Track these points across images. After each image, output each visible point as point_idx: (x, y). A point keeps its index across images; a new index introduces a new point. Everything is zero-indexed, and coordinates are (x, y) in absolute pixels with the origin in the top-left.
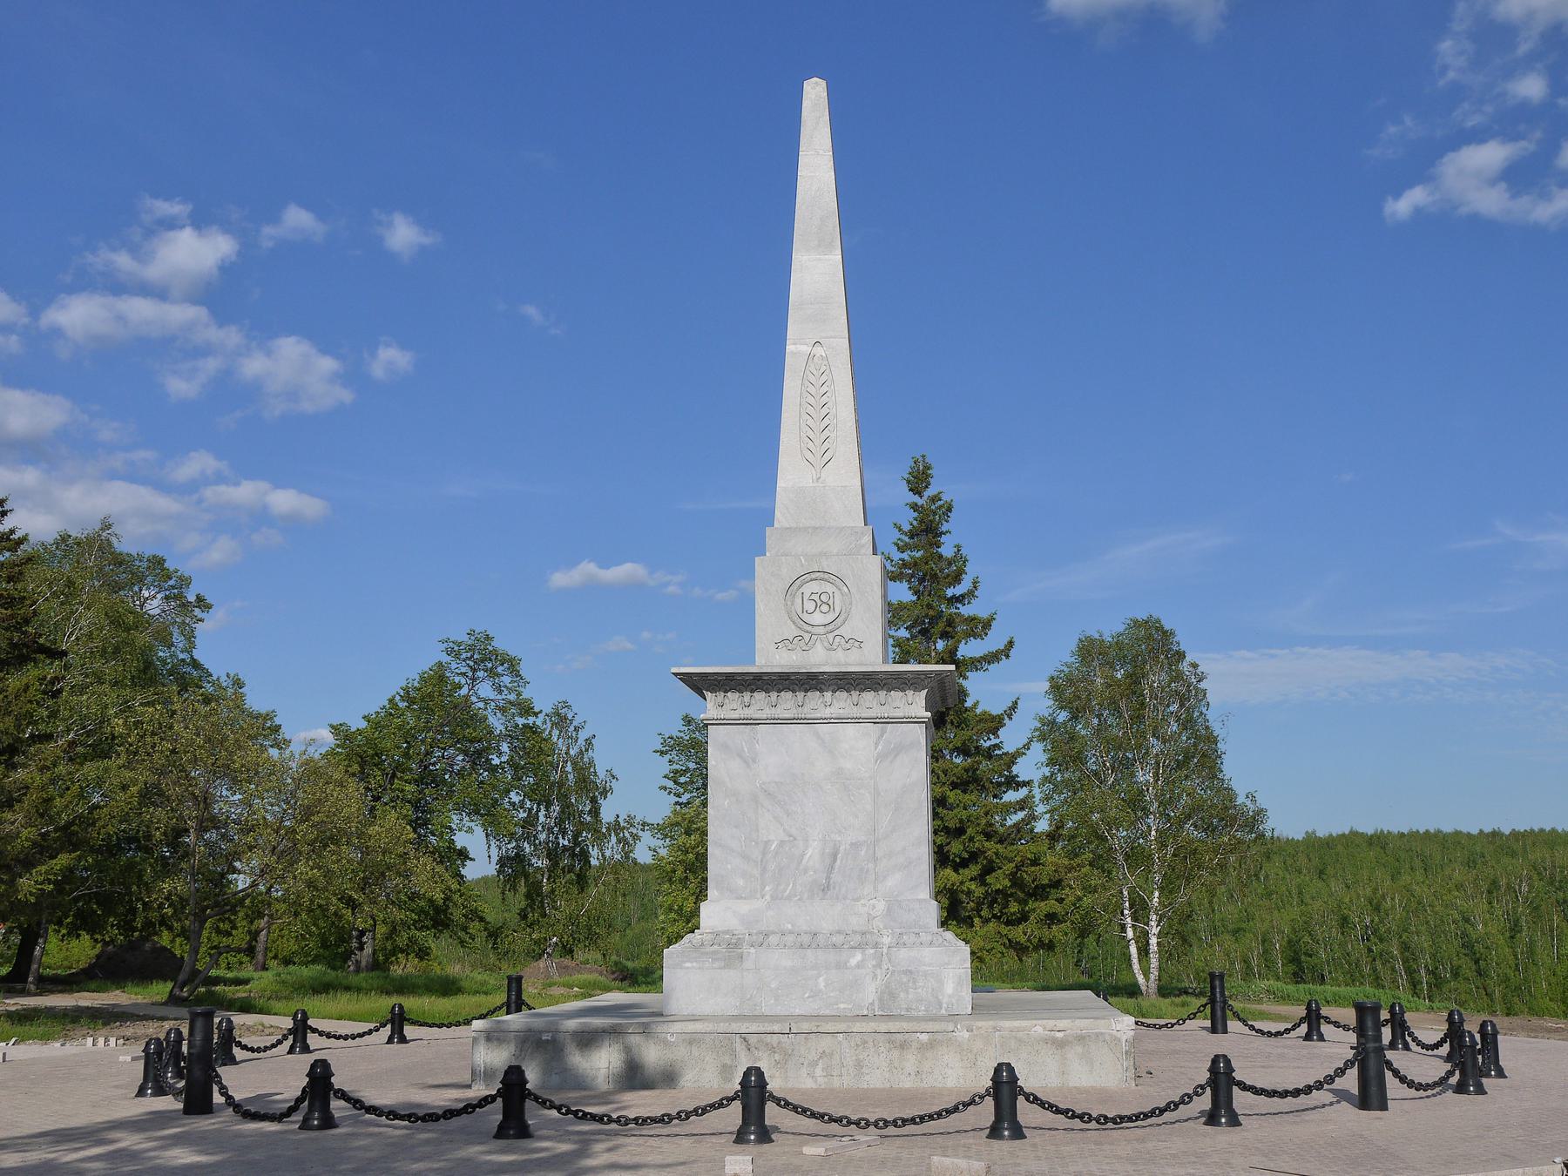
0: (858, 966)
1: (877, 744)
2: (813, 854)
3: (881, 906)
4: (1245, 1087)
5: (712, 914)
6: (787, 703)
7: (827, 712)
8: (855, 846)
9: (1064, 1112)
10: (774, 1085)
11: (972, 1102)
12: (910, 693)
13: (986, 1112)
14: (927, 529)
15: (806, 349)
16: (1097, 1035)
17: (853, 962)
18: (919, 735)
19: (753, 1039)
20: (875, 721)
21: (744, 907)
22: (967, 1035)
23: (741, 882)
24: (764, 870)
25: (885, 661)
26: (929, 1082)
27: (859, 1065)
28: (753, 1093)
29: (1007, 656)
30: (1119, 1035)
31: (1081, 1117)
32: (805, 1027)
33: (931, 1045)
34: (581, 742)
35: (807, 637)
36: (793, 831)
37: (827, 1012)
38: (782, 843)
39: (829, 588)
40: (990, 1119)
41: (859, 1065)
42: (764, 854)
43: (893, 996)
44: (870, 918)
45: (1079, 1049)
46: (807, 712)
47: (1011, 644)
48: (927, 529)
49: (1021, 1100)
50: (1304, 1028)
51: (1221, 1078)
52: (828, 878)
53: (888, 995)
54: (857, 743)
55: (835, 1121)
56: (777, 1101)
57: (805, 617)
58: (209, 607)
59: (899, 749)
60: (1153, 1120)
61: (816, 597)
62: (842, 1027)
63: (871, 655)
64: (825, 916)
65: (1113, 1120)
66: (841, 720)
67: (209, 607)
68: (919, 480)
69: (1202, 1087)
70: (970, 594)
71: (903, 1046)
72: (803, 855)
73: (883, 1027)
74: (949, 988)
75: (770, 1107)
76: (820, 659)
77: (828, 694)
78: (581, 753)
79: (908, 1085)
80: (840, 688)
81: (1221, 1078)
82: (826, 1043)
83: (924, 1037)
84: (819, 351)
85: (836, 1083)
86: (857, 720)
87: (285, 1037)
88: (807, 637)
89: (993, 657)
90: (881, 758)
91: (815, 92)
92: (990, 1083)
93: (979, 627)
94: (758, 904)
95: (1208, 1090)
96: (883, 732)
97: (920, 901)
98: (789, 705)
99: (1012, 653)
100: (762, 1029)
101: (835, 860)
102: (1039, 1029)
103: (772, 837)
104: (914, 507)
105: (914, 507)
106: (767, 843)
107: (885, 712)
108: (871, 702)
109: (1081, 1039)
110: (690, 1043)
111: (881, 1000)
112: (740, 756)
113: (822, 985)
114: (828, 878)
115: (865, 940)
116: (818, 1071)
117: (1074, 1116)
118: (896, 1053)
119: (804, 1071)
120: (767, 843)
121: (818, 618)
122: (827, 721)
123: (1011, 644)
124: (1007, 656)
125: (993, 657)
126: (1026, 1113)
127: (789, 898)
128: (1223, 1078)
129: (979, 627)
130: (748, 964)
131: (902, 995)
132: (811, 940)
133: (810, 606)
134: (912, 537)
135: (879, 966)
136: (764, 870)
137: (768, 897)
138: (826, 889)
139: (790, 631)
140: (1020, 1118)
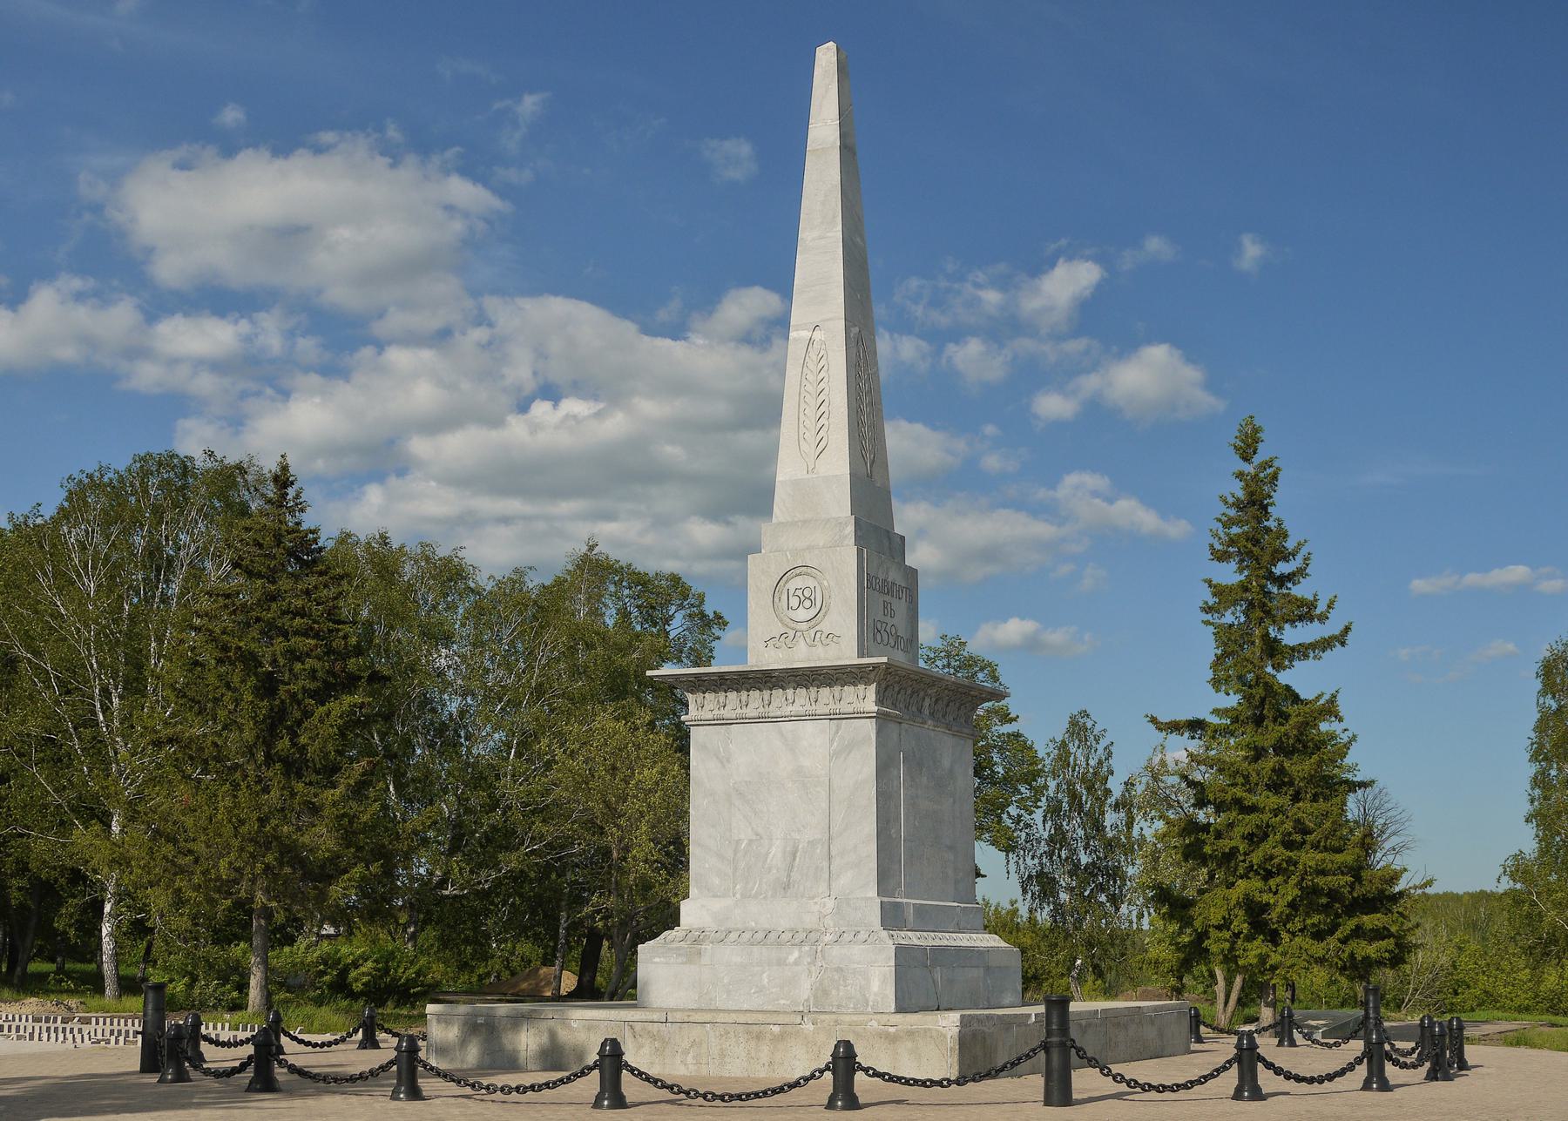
0: (796, 963)
1: (832, 741)
2: (776, 852)
3: (830, 903)
5: (691, 912)
6: (755, 701)
7: (788, 710)
14: (1255, 502)
15: (806, 334)
16: (926, 1030)
17: (792, 959)
18: (870, 727)
19: (638, 1027)
20: (833, 717)
21: (717, 905)
22: (812, 1027)
23: (717, 881)
24: (735, 869)
25: (861, 655)
27: (722, 1055)
29: (1343, 644)
30: (944, 1031)
31: (671, 1088)
32: (679, 1017)
33: (782, 1037)
34: (1101, 748)
38: (751, 841)
39: (811, 583)
41: (722, 1055)
42: (736, 852)
43: (826, 993)
44: (821, 917)
45: (909, 1044)
46: (773, 711)
47: (1347, 629)
48: (1255, 502)
52: (789, 876)
53: (822, 992)
58: (726, 624)
60: (756, 1102)
61: (799, 593)
62: (707, 1017)
63: (845, 652)
64: (783, 914)
65: (722, 1098)
66: (800, 718)
67: (726, 624)
68: (1247, 446)
70: (1301, 572)
71: (759, 1037)
72: (768, 853)
74: (875, 986)
75: (859, 1077)
76: (801, 656)
77: (790, 692)
78: (1100, 762)
79: (762, 1075)
80: (799, 685)
82: (696, 1031)
83: (776, 1029)
84: (818, 335)
85: (704, 1072)
86: (814, 717)
89: (1326, 644)
90: (834, 755)
91: (826, 57)
93: (1305, 612)
94: (729, 902)
96: (838, 728)
98: (853, 698)
99: (1350, 638)
100: (644, 1018)
102: (874, 1023)
104: (1240, 475)
105: (1240, 475)
106: (738, 842)
107: (845, 708)
108: (826, 698)
109: (911, 1034)
111: (815, 997)
114: (789, 876)
115: (806, 938)
116: (690, 1059)
117: (663, 1086)
118: (753, 1043)
119: (678, 1059)
121: (802, 614)
123: (1347, 629)
124: (1343, 644)
125: (1326, 644)
126: (630, 1087)
129: (1305, 612)
130: (705, 960)
131: (834, 992)
132: (766, 937)
133: (794, 602)
134: (1240, 509)
135: (813, 963)
136: (735, 869)
138: (786, 887)
139: (778, 629)
140: (857, 1090)
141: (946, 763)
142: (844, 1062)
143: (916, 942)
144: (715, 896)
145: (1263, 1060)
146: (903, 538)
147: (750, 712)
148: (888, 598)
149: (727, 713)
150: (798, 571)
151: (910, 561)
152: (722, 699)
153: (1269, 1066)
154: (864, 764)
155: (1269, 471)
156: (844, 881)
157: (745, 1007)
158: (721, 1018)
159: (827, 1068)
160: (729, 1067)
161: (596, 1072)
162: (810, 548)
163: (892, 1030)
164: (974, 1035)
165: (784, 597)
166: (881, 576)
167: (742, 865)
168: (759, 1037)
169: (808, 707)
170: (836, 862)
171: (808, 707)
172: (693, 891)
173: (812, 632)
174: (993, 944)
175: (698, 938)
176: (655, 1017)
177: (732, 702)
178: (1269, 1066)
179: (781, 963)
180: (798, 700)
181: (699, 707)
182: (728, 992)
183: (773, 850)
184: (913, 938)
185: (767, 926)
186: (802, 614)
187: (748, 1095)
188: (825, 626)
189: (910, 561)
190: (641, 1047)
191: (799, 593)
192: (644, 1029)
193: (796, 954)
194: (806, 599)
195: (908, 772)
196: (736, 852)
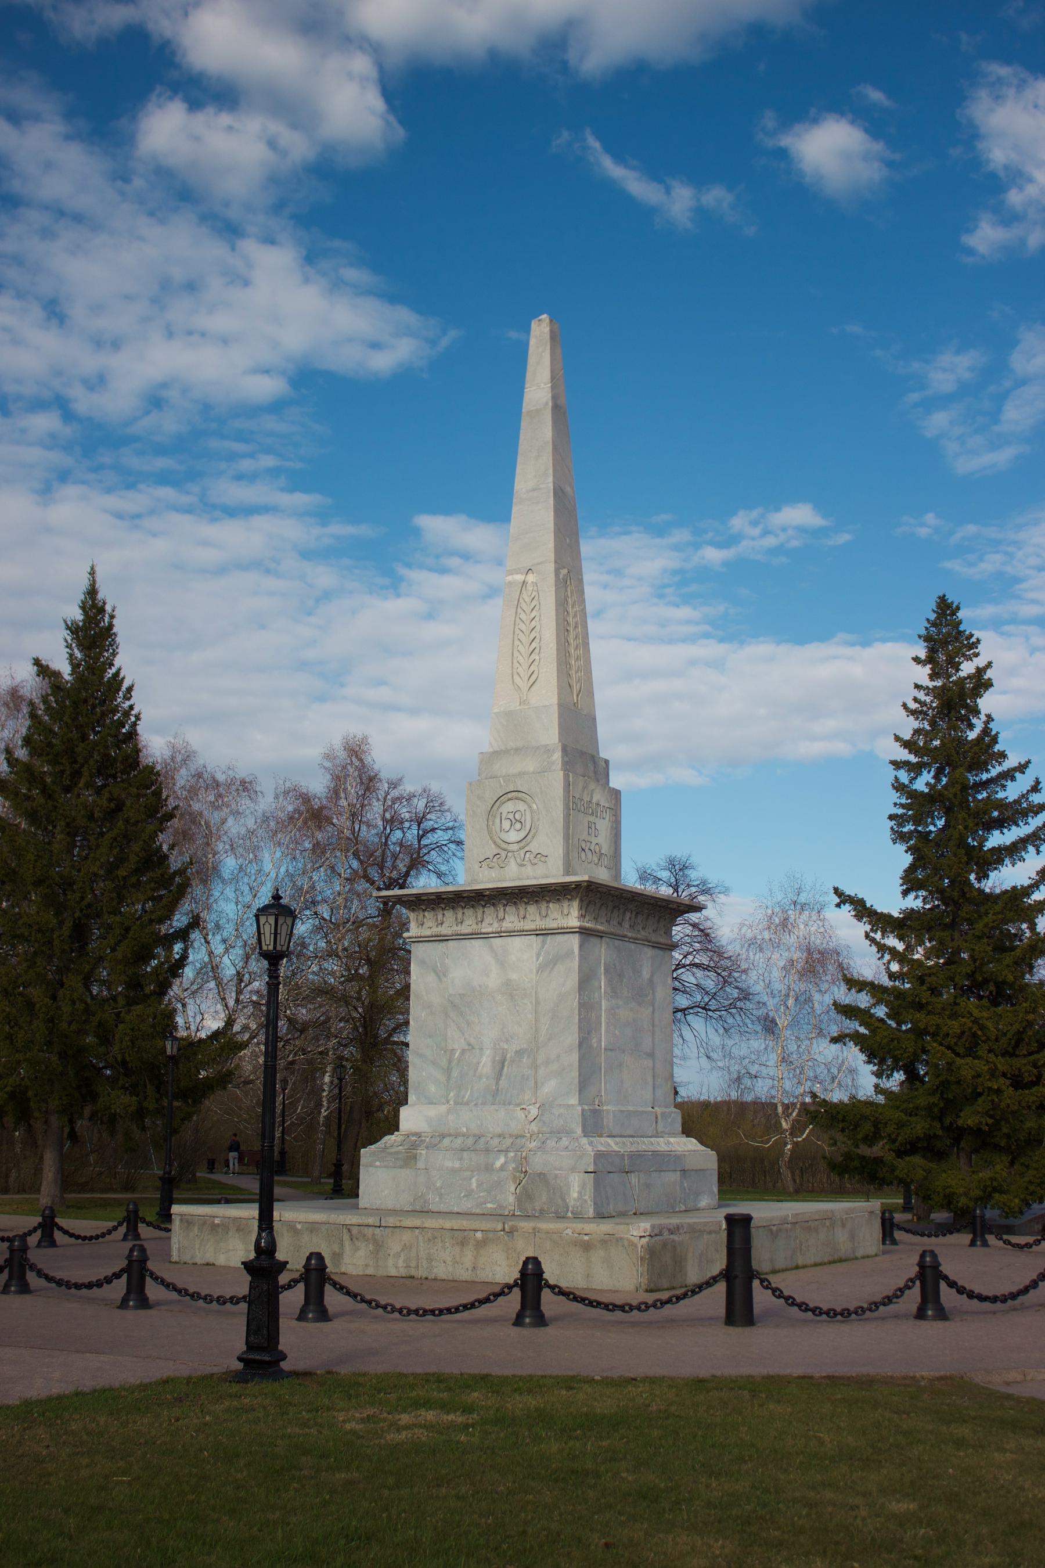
0: (502, 1168)
1: (538, 955)
2: (486, 1062)
4: (156, 1278)
5: (410, 1118)
6: (469, 921)
8: (519, 1053)
9: (354, 1296)
10: (551, 1274)
11: (502, 1293)
12: (566, 904)
13: (513, 1301)
17: (498, 1164)
19: (355, 1230)
20: (543, 933)
21: (433, 1111)
25: (567, 872)
26: (484, 1275)
28: (314, 1276)
35: (503, 854)
36: (472, 1041)
37: (478, 1211)
38: (463, 1051)
39: (521, 806)
40: (914, 1308)
42: (450, 1062)
45: (602, 1253)
49: (328, 1288)
50: (123, 1229)
51: (929, 1275)
54: (523, 953)
55: (810, 1310)
56: (334, 1284)
57: (503, 836)
59: (552, 962)
60: (449, 1317)
61: (511, 816)
66: (511, 933)
69: (912, 1280)
71: (463, 1243)
72: (479, 1063)
73: (448, 1224)
75: (546, 1295)
76: (513, 876)
81: (929, 1275)
82: (407, 1236)
84: (531, 578)
86: (522, 933)
87: (120, 1224)
88: (503, 854)
90: (541, 969)
91: (540, 329)
92: (518, 1275)
94: (443, 1108)
95: (918, 1283)
96: (544, 943)
97: (569, 1106)
100: (360, 1221)
101: (503, 1068)
103: (456, 1046)
106: (453, 1051)
108: (534, 917)
110: (311, 1232)
112: (435, 971)
113: (474, 1185)
118: (458, 1249)
120: (453, 1051)
122: (499, 934)
127: (467, 1104)
128: (928, 1271)
130: (421, 1164)
133: (506, 825)
137: (451, 1102)
139: (491, 850)
140: (544, 1308)
141: (646, 974)
142: (531, 1279)
143: (615, 1148)
144: (432, 1103)
145: (946, 1278)
146: (607, 762)
147: (465, 929)
148: (592, 819)
149: (444, 930)
150: (509, 796)
151: (613, 784)
152: (460, 915)
153: (952, 1284)
154: (565, 979)
155: (1010, 549)
156: (549, 1087)
157: (456, 1209)
158: (430, 1223)
159: (516, 1284)
160: (435, 1271)
161: (301, 1286)
162: (521, 774)
163: (586, 1238)
164: (665, 1244)
165: (498, 820)
166: (586, 798)
167: (455, 1073)
168: (463, 1243)
169: (455, 928)
170: (542, 1071)
171: (475, 926)
172: (412, 1098)
173: (522, 852)
174: (690, 1147)
175: (416, 1141)
176: (370, 1221)
177: (448, 922)
178: (952, 1284)
179: (489, 1168)
180: (511, 918)
181: (419, 926)
182: (441, 1196)
183: (484, 1059)
184: (613, 1145)
185: (477, 1132)
186: (513, 836)
187: (441, 1311)
188: (534, 847)
189: (613, 784)
190: (357, 1249)
191: (511, 816)
192: (360, 1232)
193: (502, 1160)
194: (516, 821)
195: (609, 981)
196: (450, 1062)
